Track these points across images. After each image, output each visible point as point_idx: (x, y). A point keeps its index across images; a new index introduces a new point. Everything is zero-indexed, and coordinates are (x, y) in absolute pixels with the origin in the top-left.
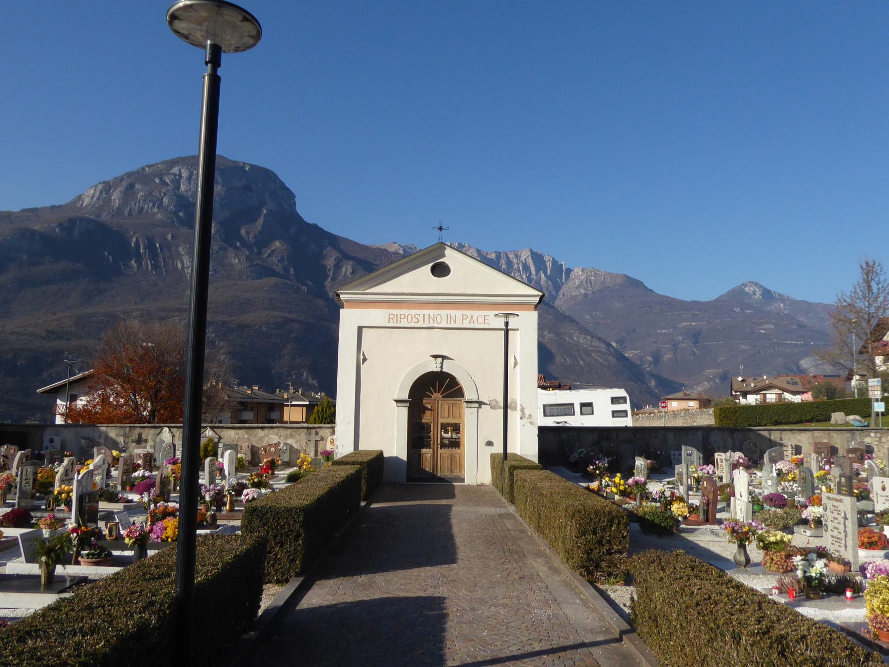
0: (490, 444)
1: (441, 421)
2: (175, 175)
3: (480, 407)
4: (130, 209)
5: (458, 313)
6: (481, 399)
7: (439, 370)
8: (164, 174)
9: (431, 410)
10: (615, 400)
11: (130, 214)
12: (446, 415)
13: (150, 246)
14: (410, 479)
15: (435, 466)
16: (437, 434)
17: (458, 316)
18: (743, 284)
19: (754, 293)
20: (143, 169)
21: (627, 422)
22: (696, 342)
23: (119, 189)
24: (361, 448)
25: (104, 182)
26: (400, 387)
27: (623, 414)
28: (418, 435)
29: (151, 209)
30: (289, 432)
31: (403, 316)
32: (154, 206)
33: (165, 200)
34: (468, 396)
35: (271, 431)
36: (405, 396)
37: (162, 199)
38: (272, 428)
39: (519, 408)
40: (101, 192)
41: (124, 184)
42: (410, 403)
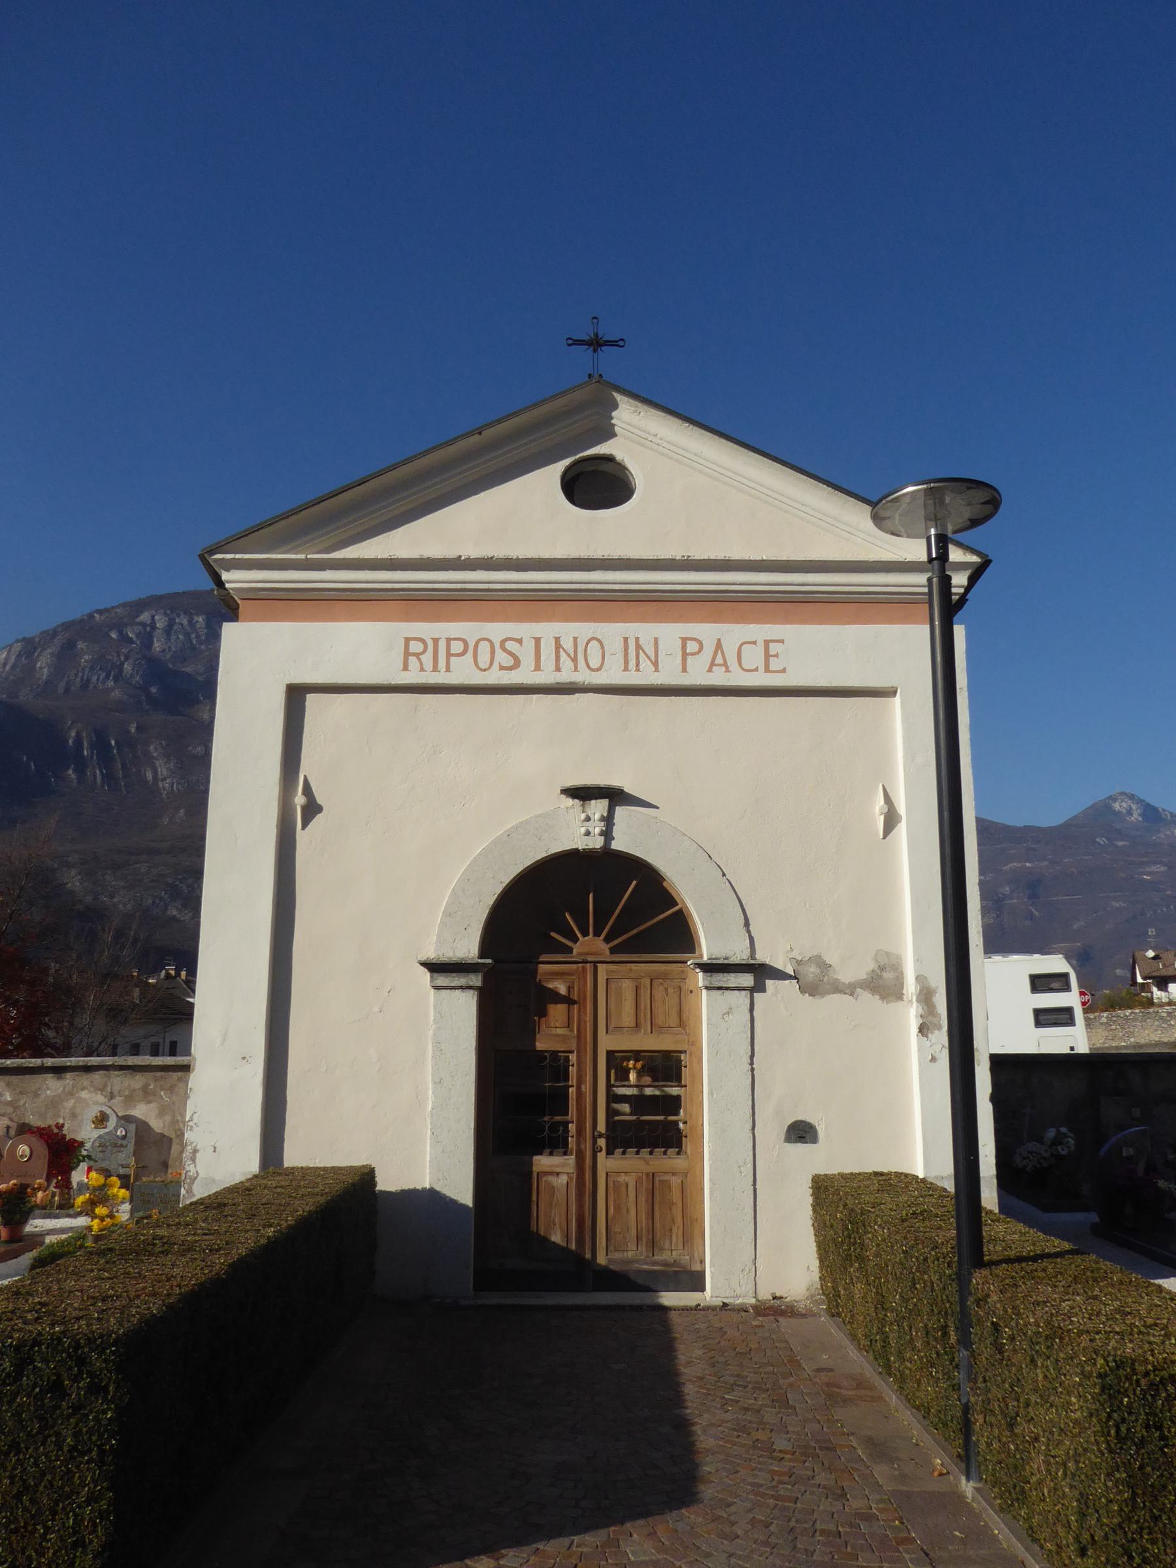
0: (801, 1132)
1: (607, 1042)
2: (143, 624)
3: (759, 987)
4: (67, 684)
5: (667, 634)
6: (762, 957)
7: (597, 843)
8: (126, 625)
9: (568, 1000)
10: (1039, 983)
11: (67, 691)
12: (628, 1019)
13: (101, 744)
14: (485, 1279)
15: (585, 1225)
16: (591, 1097)
17: (668, 646)
18: (1110, 798)
19: (1130, 812)
20: (91, 616)
21: (1074, 1039)
22: (1033, 896)
23: (49, 651)
24: (294, 1156)
25: (24, 639)
26: (447, 914)
27: (1062, 1017)
28: (517, 1100)
29: (103, 682)
30: (137, 1081)
31: (457, 647)
32: (108, 677)
33: (127, 667)
34: (707, 950)
35: (85, 1079)
36: (467, 945)
37: (122, 664)
38: (87, 1069)
39: (911, 987)
40: (19, 656)
41: (59, 641)
42: (490, 975)
